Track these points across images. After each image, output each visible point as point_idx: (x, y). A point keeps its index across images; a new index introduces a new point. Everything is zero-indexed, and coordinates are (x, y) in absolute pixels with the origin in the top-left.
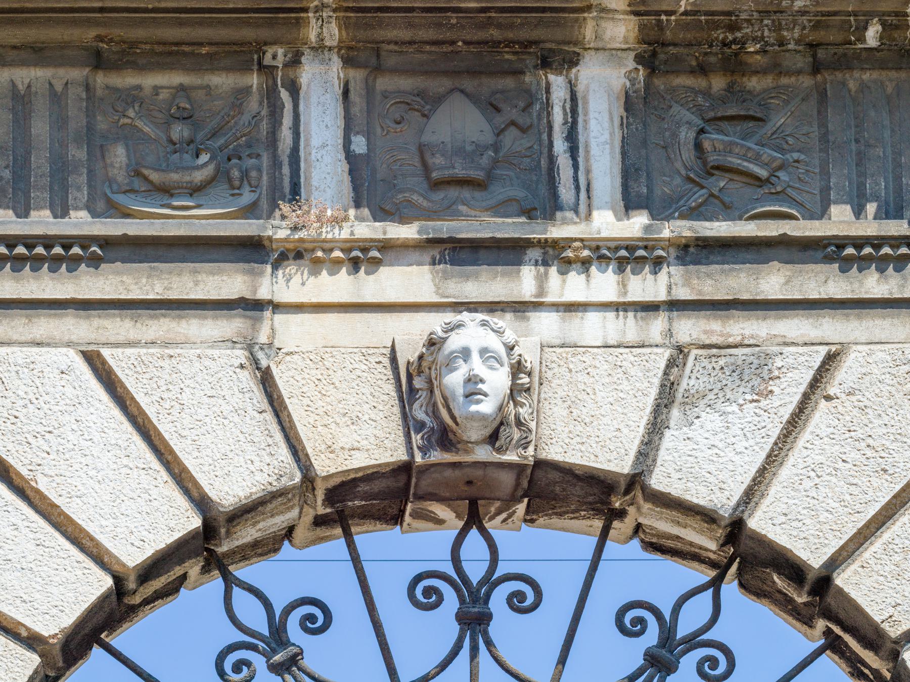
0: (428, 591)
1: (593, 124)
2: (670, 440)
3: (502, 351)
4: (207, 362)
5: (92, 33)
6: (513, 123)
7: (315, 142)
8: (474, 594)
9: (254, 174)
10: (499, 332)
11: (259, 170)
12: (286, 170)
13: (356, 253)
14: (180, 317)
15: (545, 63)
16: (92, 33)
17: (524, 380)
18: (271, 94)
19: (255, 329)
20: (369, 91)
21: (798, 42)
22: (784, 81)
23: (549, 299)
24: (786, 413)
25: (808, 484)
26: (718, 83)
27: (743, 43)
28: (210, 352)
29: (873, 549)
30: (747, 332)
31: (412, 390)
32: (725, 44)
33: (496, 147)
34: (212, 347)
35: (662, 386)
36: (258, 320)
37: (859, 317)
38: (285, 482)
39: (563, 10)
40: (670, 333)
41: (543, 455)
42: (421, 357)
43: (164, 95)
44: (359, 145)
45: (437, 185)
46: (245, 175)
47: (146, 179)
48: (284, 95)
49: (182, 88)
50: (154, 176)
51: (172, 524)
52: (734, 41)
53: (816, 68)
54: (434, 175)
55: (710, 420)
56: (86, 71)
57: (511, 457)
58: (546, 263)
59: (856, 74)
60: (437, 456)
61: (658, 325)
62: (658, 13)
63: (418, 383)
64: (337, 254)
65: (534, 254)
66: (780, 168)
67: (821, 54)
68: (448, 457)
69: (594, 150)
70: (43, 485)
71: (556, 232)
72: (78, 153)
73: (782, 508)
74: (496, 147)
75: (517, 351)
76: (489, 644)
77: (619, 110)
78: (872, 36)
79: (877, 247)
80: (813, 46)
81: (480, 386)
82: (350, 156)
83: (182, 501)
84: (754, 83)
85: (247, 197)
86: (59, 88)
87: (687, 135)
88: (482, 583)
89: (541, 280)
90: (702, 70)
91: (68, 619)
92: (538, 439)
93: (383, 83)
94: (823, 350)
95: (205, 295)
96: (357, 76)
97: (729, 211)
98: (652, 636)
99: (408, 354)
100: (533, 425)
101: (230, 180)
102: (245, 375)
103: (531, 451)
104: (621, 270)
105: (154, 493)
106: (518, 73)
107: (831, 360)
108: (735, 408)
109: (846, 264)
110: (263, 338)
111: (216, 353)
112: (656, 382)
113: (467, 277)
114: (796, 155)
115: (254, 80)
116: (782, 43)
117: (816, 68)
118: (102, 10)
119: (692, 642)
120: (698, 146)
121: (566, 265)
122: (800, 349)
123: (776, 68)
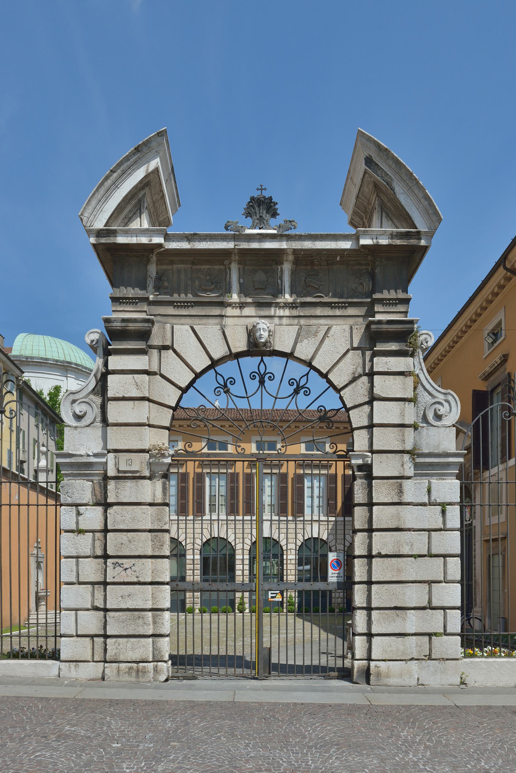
0: (254, 376)
1: (285, 276)
2: (298, 345)
3: (267, 328)
4: (213, 329)
5: (192, 258)
6: (270, 276)
7: (233, 280)
8: (262, 376)
9: (222, 287)
10: (266, 325)
11: (223, 286)
12: (228, 286)
13: (241, 305)
14: (208, 319)
15: (277, 264)
16: (192, 258)
17: (271, 333)
18: (226, 269)
19: (222, 321)
20: (244, 269)
21: (324, 260)
22: (322, 267)
23: (277, 315)
24: (320, 340)
25: (323, 355)
26: (309, 267)
27: (314, 260)
28: (213, 326)
29: (335, 369)
30: (314, 322)
31: (250, 335)
32: (310, 260)
33: (267, 281)
34: (214, 325)
35: (297, 334)
36: (222, 320)
37: (335, 319)
38: (227, 354)
39: (280, 254)
40: (299, 322)
41: (274, 349)
42: (252, 329)
43: (206, 270)
44: (242, 281)
45: (256, 289)
46: (220, 288)
47: (202, 288)
48: (228, 270)
49: (209, 268)
50: (203, 287)
51: (206, 363)
52: (312, 260)
53: (328, 264)
54: (255, 287)
55: (306, 341)
56: (191, 265)
57: (268, 349)
58: (276, 307)
59: (335, 266)
60: (255, 349)
61: (296, 321)
62: (298, 255)
63: (251, 334)
64: (237, 305)
65: (274, 305)
66: (321, 286)
67: (329, 262)
68: (257, 349)
69: (286, 282)
70: (182, 355)
71: (278, 300)
72: (189, 282)
73: (318, 360)
74: (267, 281)
75: (270, 328)
76: (265, 387)
77: (290, 273)
78: (338, 259)
79: (338, 304)
80: (327, 260)
81: (262, 336)
82: (240, 283)
83: (208, 358)
84: (316, 268)
85: (221, 292)
86: (186, 269)
87: (303, 278)
88: (263, 374)
89: (275, 311)
90: (306, 265)
91: (187, 384)
92: (273, 345)
93: (246, 268)
94: (327, 327)
95: (69, 562)
96: (241, 266)
97: (310, 295)
98: (295, 386)
99: (250, 328)
100: (272, 343)
101: (217, 288)
102: (219, 331)
103: (272, 348)
104: (289, 309)
105: (202, 356)
106: (271, 265)
107: (329, 329)
108: (310, 339)
109: (332, 308)
110: (224, 323)
111: (215, 326)
112: (296, 333)
113: (261, 310)
114: (323, 283)
115: (222, 267)
116: (321, 260)
117: (328, 264)
118: (194, 254)
119: (303, 387)
120: (305, 281)
121: (280, 307)
122: (323, 327)
123: (320, 265)
